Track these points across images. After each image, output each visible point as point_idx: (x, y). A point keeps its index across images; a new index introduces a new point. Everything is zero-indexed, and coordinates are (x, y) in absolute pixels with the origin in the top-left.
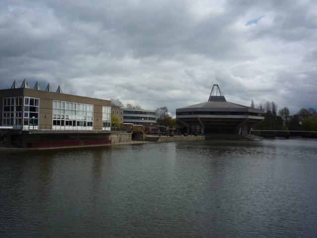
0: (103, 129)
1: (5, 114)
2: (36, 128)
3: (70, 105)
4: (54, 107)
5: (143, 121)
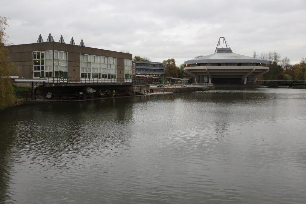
1: (35, 67)
4: (125, 65)
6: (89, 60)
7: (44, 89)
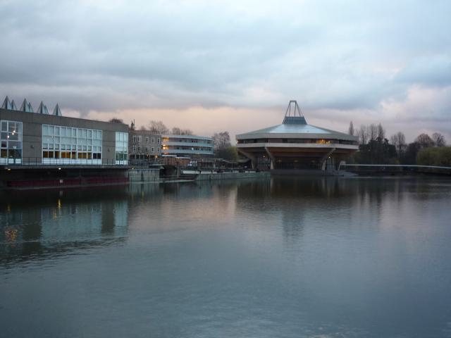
0: (117, 163)
2: (18, 161)
3: (83, 132)
5: (193, 151)
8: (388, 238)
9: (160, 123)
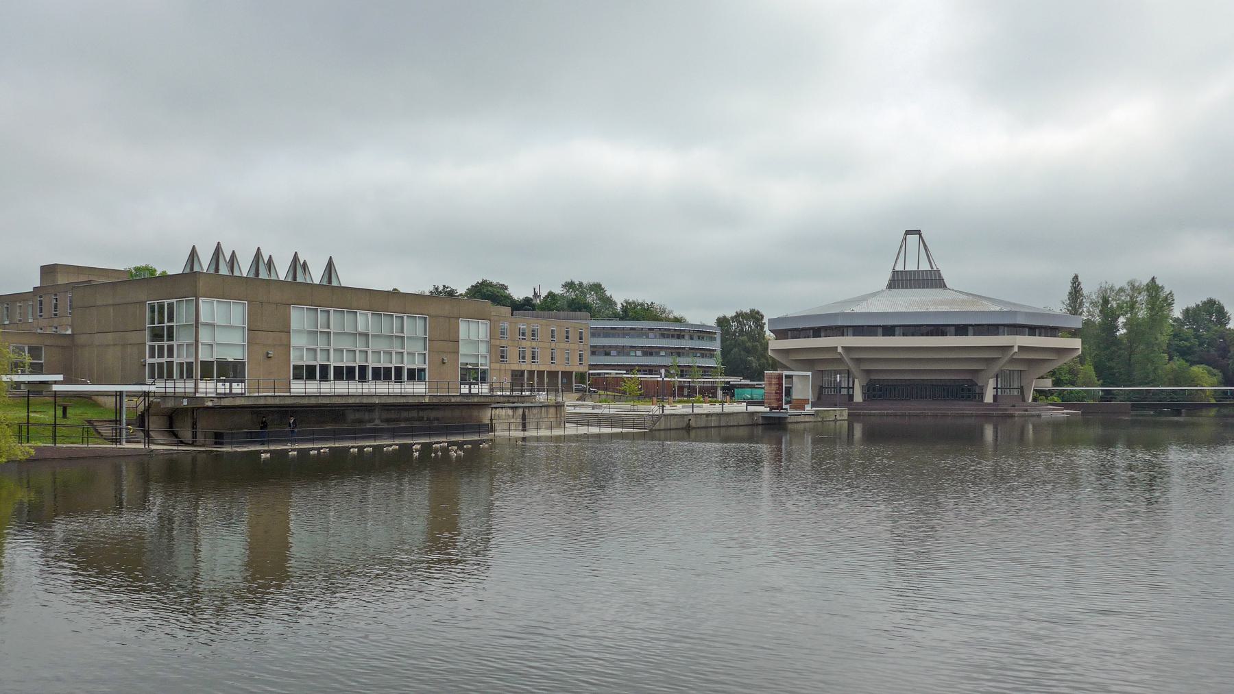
0: (465, 390)
1: (152, 348)
2: (237, 388)
4: (461, 337)
6: (361, 329)
7: (175, 417)
8: (1057, 580)
9: (597, 288)
